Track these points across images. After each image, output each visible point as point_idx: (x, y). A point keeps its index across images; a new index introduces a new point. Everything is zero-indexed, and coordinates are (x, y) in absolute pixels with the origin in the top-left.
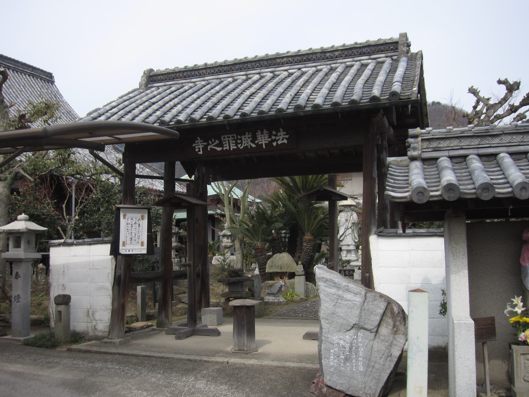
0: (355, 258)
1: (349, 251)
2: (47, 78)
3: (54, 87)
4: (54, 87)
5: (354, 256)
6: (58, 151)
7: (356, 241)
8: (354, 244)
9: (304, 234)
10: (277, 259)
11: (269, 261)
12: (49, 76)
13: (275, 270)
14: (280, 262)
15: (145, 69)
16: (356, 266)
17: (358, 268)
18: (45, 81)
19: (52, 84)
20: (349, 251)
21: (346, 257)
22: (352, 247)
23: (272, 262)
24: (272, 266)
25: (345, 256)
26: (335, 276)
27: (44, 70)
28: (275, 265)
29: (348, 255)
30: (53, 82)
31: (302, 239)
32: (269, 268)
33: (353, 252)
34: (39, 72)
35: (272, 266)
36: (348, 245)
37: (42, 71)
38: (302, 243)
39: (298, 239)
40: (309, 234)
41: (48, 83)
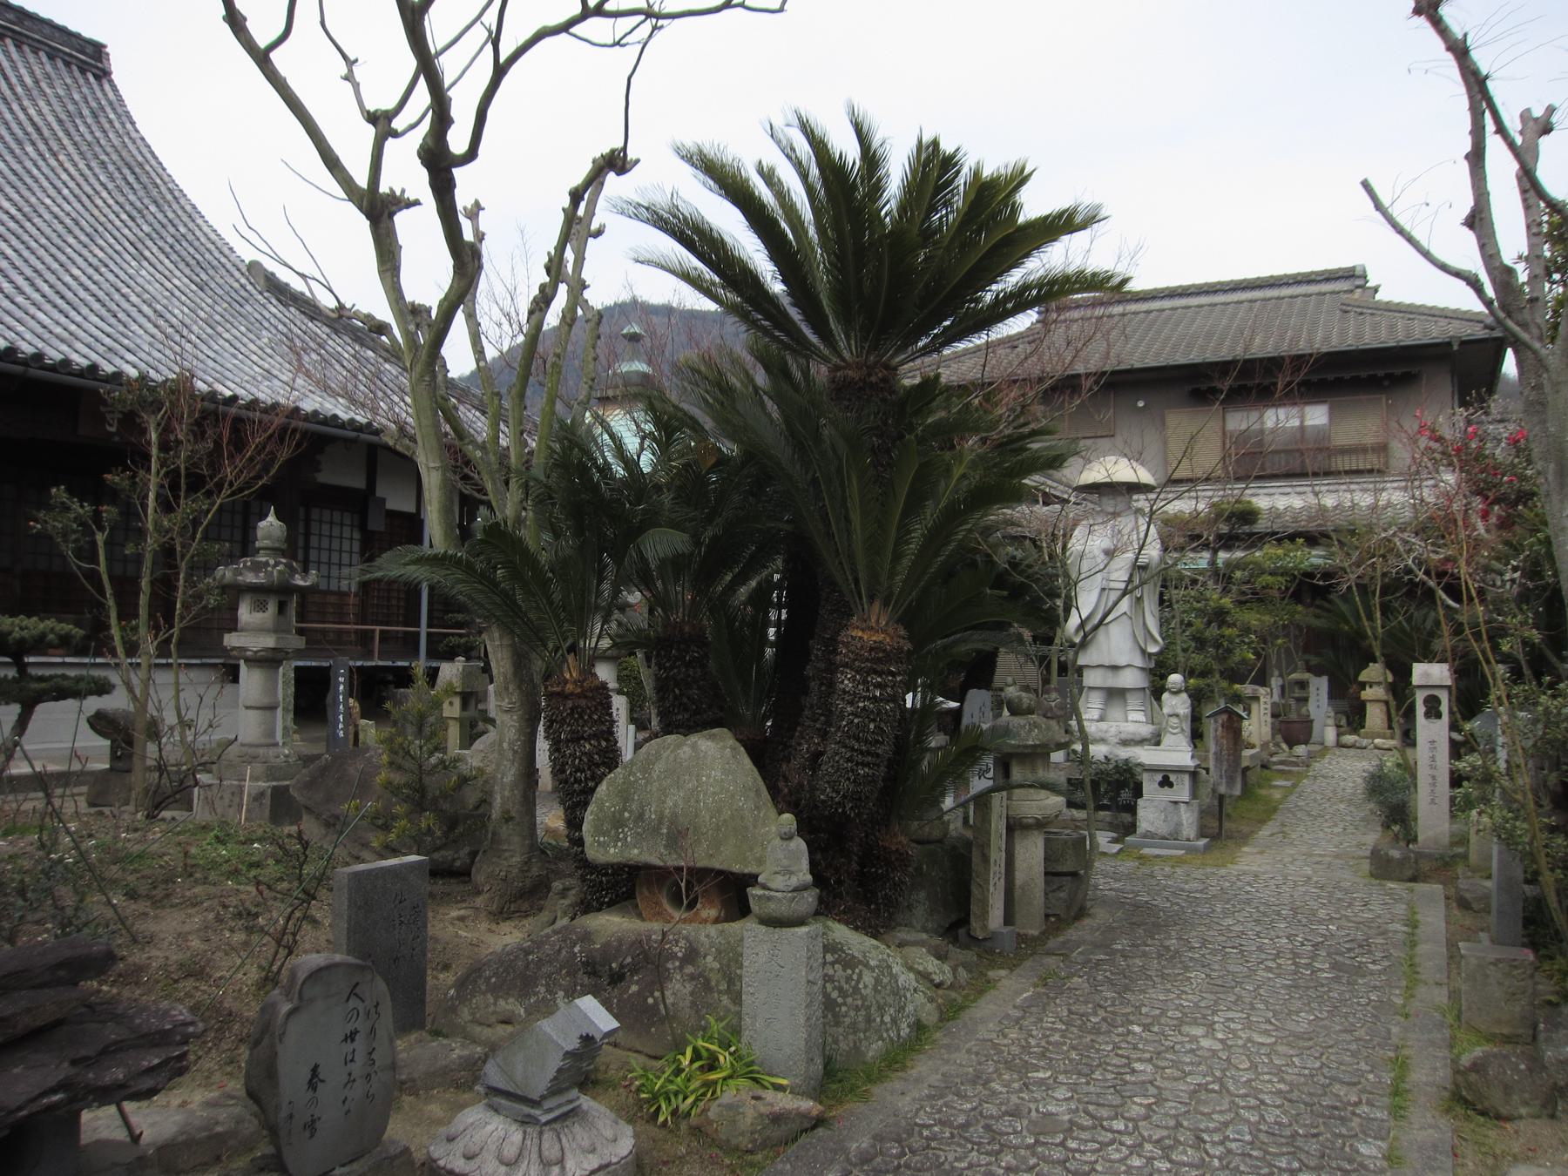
0: (1146, 730)
1: (1115, 695)
2: (88, 59)
3: (107, 87)
4: (107, 87)
5: (1140, 717)
6: (1391, 698)
7: (1153, 649)
8: (1138, 661)
9: (845, 612)
10: (659, 767)
11: (603, 788)
12: (89, 50)
13: (636, 854)
14: (674, 800)
15: (598, 155)
16: (1153, 770)
17: (1159, 777)
18: (67, 64)
19: (97, 77)
20: (1115, 695)
21: (1102, 719)
22: (1131, 679)
23: (625, 795)
24: (618, 823)
25: (1095, 714)
26: (926, 1070)
27: (73, 28)
28: (640, 817)
29: (1115, 712)
30: (103, 74)
31: (832, 645)
32: (598, 831)
33: (1133, 701)
34: (47, 30)
35: (618, 823)
36: (1115, 668)
37: (63, 30)
38: (832, 668)
39: (817, 649)
40: (878, 615)
41: (83, 72)
